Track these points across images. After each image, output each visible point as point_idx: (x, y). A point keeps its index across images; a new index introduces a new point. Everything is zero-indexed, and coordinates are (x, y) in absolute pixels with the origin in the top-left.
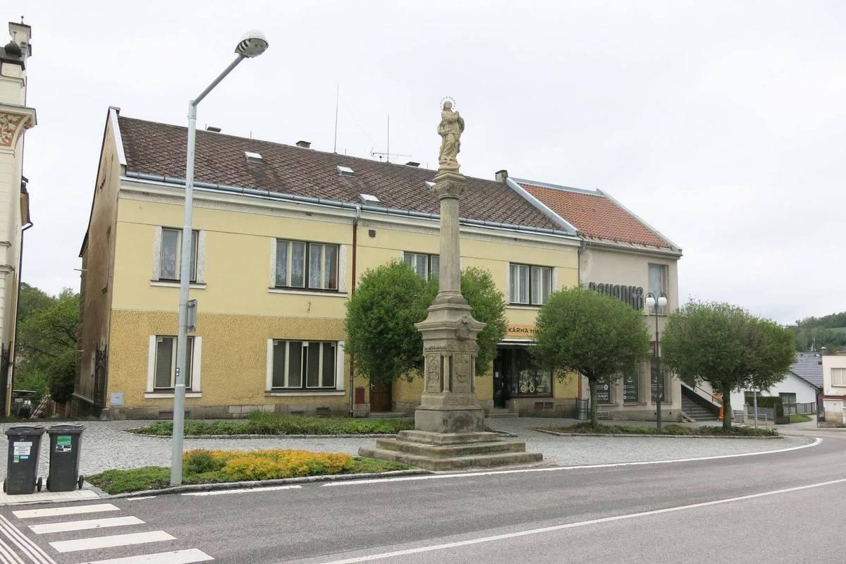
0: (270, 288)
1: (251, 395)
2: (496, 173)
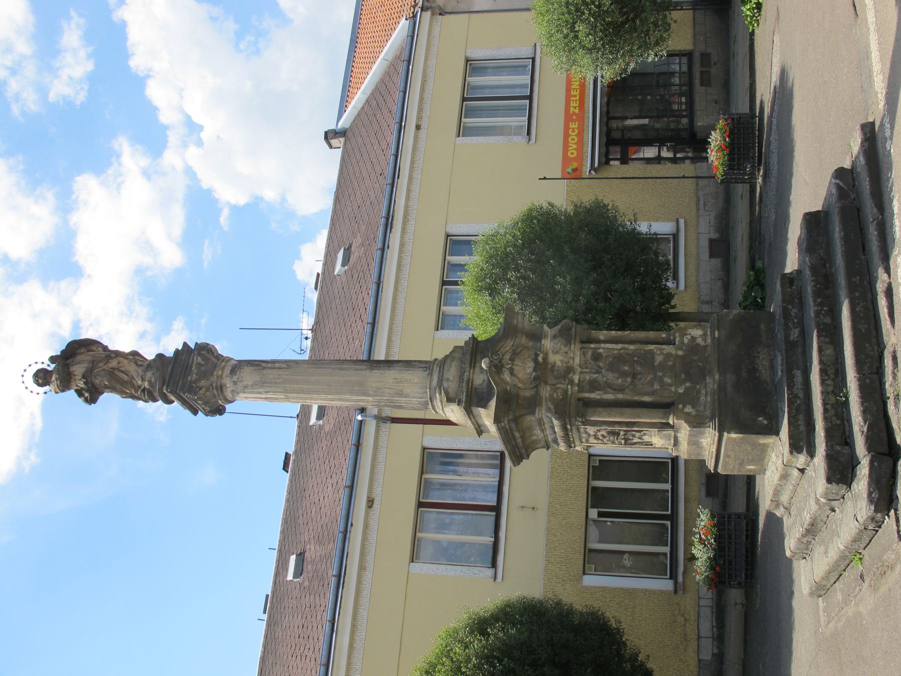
0: (495, 578)
1: (680, 619)
2: (331, 147)
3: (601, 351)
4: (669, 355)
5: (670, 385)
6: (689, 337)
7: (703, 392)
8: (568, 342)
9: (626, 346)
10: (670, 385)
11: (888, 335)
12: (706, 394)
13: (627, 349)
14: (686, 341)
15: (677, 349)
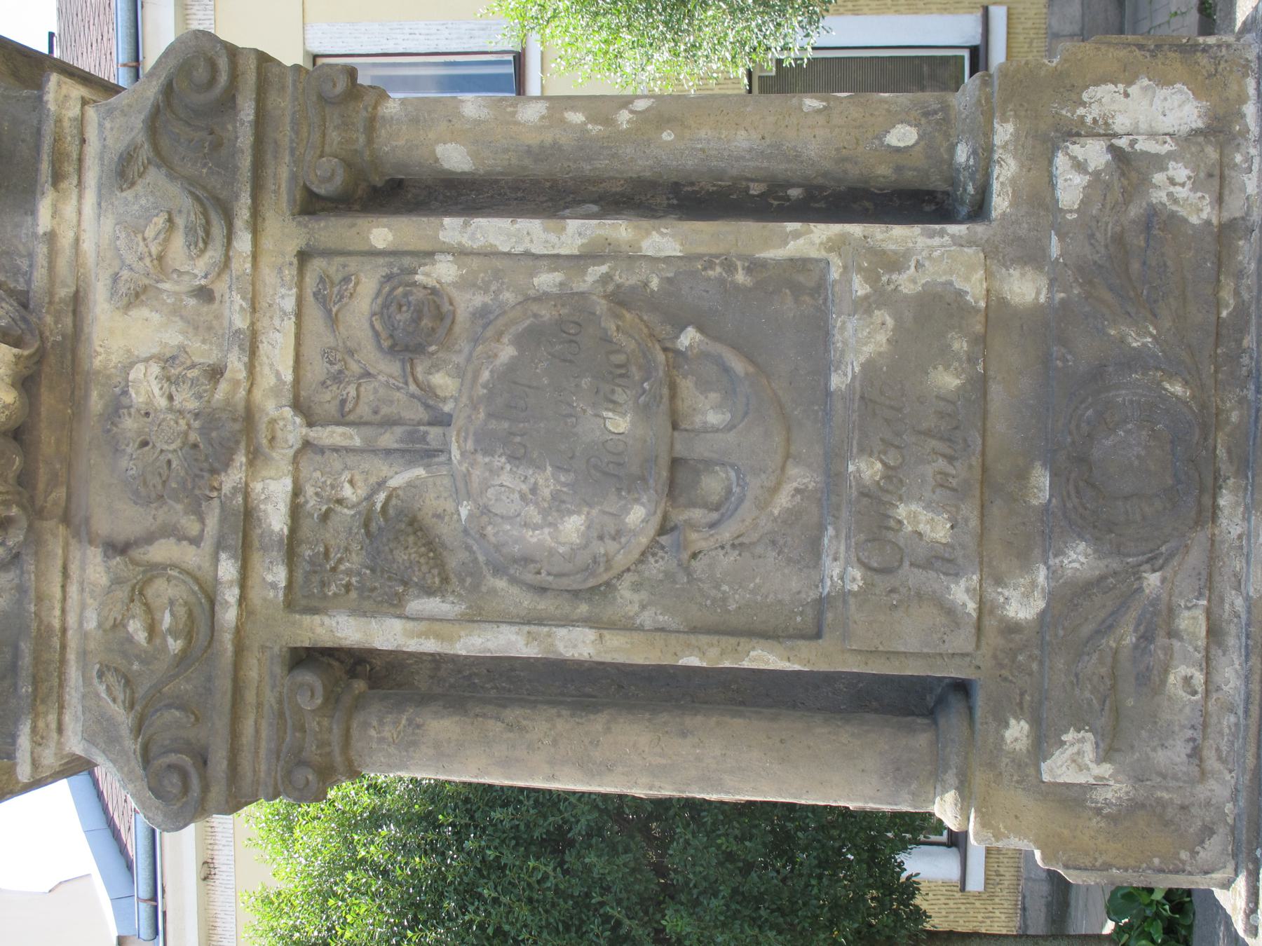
3: (444, 271)
4: (936, 310)
5: (942, 561)
6: (1094, 153)
7: (1192, 621)
8: (214, 209)
9: (621, 230)
10: (942, 561)
11: (580, 654)
12: (1215, 632)
13: (633, 258)
14: (1070, 189)
15: (994, 255)
